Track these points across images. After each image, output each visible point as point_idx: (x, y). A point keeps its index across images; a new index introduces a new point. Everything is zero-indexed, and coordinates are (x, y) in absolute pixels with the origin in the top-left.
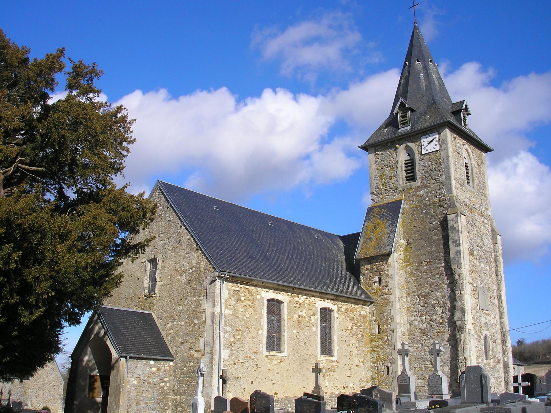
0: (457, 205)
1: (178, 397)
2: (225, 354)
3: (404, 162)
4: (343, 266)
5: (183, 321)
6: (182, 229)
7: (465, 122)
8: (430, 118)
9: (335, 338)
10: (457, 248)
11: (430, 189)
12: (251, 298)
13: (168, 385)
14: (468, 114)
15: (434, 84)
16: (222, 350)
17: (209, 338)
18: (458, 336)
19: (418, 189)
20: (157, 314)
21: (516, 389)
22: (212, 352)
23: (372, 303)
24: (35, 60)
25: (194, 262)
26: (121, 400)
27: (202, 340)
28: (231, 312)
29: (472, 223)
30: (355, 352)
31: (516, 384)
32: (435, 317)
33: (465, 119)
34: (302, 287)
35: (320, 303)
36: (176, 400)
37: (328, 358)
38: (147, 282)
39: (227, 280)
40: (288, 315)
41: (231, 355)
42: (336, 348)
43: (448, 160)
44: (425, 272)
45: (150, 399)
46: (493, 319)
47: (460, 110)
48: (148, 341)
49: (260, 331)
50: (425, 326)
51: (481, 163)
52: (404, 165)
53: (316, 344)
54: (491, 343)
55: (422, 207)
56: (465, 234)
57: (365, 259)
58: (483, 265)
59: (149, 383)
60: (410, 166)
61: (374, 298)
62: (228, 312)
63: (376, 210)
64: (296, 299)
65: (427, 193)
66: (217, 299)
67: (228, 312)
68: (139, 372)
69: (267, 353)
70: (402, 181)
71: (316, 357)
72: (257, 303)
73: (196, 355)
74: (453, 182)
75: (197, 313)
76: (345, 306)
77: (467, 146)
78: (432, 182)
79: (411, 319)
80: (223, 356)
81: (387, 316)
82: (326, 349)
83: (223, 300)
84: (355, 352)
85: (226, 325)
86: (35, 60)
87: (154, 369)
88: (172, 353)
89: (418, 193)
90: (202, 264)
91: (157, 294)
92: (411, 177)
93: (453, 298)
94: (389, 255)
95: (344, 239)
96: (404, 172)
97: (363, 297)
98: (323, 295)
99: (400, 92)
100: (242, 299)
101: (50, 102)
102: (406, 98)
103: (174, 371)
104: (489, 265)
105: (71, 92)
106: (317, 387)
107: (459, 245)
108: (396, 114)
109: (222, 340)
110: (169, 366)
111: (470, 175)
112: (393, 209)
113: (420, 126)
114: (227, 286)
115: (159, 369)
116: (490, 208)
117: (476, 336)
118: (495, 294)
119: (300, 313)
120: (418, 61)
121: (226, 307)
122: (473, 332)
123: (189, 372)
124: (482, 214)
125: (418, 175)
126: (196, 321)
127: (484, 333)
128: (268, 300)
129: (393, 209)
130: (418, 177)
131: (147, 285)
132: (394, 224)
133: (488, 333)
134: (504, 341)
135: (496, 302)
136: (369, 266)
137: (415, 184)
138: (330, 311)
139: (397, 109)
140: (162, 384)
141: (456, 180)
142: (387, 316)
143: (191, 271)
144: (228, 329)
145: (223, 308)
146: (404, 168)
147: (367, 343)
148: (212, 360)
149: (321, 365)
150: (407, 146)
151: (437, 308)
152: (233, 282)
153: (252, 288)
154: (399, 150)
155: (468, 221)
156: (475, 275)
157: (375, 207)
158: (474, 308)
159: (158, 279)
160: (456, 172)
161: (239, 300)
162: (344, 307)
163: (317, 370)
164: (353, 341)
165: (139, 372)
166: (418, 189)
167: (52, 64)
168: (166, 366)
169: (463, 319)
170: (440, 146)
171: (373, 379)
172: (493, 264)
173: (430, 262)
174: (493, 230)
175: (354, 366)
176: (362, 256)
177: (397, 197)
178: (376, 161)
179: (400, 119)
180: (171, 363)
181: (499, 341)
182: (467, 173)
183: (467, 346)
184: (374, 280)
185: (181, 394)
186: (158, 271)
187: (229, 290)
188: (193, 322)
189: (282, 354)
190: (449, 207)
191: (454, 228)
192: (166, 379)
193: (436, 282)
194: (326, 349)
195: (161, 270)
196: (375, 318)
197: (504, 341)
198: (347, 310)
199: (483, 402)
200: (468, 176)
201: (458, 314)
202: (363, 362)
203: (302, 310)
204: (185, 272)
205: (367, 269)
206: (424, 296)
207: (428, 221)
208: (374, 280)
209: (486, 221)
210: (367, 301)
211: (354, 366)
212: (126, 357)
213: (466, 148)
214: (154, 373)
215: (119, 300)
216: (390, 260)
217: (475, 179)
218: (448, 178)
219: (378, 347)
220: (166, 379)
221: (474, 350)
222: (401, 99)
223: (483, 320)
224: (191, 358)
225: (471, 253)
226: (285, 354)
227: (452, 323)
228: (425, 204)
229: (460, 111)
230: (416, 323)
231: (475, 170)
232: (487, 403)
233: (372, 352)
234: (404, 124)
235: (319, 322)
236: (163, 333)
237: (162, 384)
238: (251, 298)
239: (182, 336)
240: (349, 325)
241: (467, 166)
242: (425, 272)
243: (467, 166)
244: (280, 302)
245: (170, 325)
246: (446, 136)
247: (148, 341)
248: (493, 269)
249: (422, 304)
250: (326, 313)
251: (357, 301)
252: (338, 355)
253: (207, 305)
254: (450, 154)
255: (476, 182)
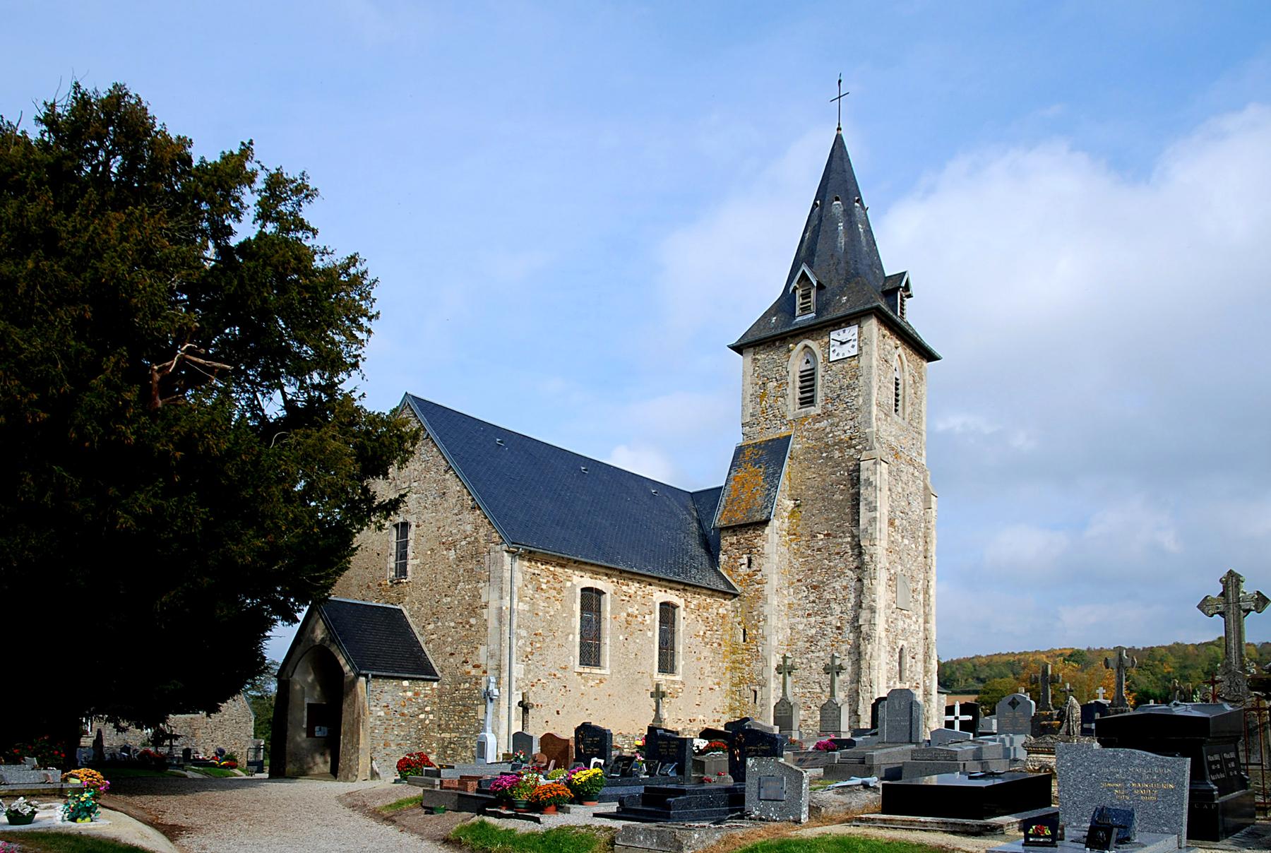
0: (877, 445)
1: (447, 735)
2: (518, 670)
3: (798, 374)
4: (685, 538)
5: (452, 620)
6: (447, 476)
7: (902, 309)
8: (848, 300)
9: (680, 648)
10: (873, 514)
11: (836, 420)
12: (558, 586)
13: (431, 716)
14: (909, 296)
15: (860, 242)
16: (514, 665)
17: (494, 647)
18: (862, 648)
19: (818, 418)
20: (410, 610)
21: (950, 725)
22: (499, 668)
23: (735, 596)
24: (203, 160)
25: (469, 528)
26: (361, 741)
27: (482, 649)
28: (526, 607)
29: (896, 475)
30: (708, 668)
31: (951, 718)
32: (830, 618)
33: (902, 305)
34: (635, 570)
35: (660, 595)
36: (443, 739)
37: (670, 677)
38: (393, 559)
39: (522, 557)
40: (612, 613)
41: (527, 671)
42: (680, 663)
43: (869, 373)
44: (819, 550)
45: (405, 738)
46: (915, 624)
47: (896, 289)
48: (397, 651)
49: (571, 637)
50: (813, 631)
51: (918, 379)
52: (798, 379)
53: (653, 657)
54: (908, 658)
55: (823, 449)
56: (886, 492)
57: (727, 528)
58: (906, 542)
59: (403, 714)
60: (808, 380)
61: (739, 589)
62: (522, 606)
63: (748, 452)
64: (625, 588)
65: (832, 425)
66: (507, 587)
67: (522, 606)
68: (387, 698)
69: (581, 670)
70: (791, 406)
71: (652, 676)
72: (565, 593)
73: (473, 672)
74: (874, 409)
75: (474, 608)
76: (696, 600)
77: (900, 350)
78: (841, 407)
79: (793, 620)
80: (514, 674)
81: (758, 615)
82: (667, 665)
83: (515, 589)
84: (708, 668)
85: (519, 626)
86: (203, 160)
87: (409, 694)
88: (436, 669)
89: (817, 425)
90: (482, 532)
91: (409, 579)
92: (807, 401)
93: (860, 593)
94: (766, 522)
95: (696, 496)
96: (798, 390)
97: (722, 587)
98: (668, 583)
99: (803, 254)
100: (544, 586)
101: (234, 242)
102: (810, 266)
103: (440, 697)
104: (916, 543)
105: (263, 226)
106: (658, 717)
107: (875, 509)
108: (794, 291)
109: (514, 649)
110: (432, 689)
111: (900, 398)
112: (775, 451)
113: (826, 317)
114: (522, 566)
115: (416, 694)
116: (924, 453)
117: (888, 648)
118: (920, 587)
119: (630, 610)
120: (837, 199)
121: (520, 600)
122: (884, 642)
123: (462, 698)
124: (911, 462)
125: (820, 395)
126: (473, 621)
127: (901, 643)
128: (583, 590)
129: (775, 451)
130: (819, 400)
131: (393, 565)
132: (776, 475)
133: (905, 643)
134: (927, 657)
135: (921, 597)
136: (734, 540)
137: (815, 410)
138: (675, 607)
139: (794, 284)
140: (422, 716)
141: (879, 405)
142: (758, 615)
143: (464, 543)
144: (523, 633)
145: (515, 601)
146: (798, 384)
147: (725, 656)
148: (499, 678)
149: (663, 688)
150: (806, 346)
151: (833, 605)
152: (529, 560)
153: (559, 570)
154: (793, 354)
155: (890, 473)
156: (894, 557)
157: (749, 446)
158: (889, 607)
159: (410, 554)
160: (880, 393)
161: (539, 589)
162: (695, 602)
163: (658, 695)
164: (706, 652)
165: (387, 698)
166: (818, 418)
167: (232, 172)
168: (428, 689)
169: (872, 624)
170: (860, 348)
171: (732, 709)
172: (921, 541)
173: (828, 535)
174: (926, 488)
175: (706, 691)
176: (723, 523)
177: (784, 431)
178: (755, 371)
179: (799, 301)
180: (435, 685)
181: (920, 657)
182: (897, 395)
183: (875, 663)
184: (741, 561)
185: (452, 731)
186: (411, 543)
187: (524, 573)
188: (468, 622)
189: (603, 672)
190: (865, 449)
191: (869, 483)
192: (428, 709)
193: (835, 567)
194: (667, 665)
195: (415, 541)
196: (739, 619)
197: (927, 657)
198: (699, 607)
199: (911, 742)
200: (897, 400)
201: (865, 615)
202: (718, 684)
203: (632, 605)
204: (454, 544)
205: (731, 544)
206: (815, 587)
207: (829, 470)
208: (741, 561)
209: (917, 474)
210: (729, 593)
211: (706, 691)
212: (366, 676)
213: (899, 352)
214: (410, 699)
215: (352, 587)
216: (767, 530)
217: (907, 404)
218: (867, 402)
219: (743, 662)
220: (428, 709)
221: (884, 667)
222: (804, 268)
223: (900, 623)
224: (466, 677)
225: (891, 523)
226: (606, 671)
227: (857, 629)
228: (827, 444)
229: (896, 290)
230: (801, 627)
231: (910, 391)
232: (917, 743)
233: (733, 669)
234: (805, 310)
235: (657, 624)
236: (420, 639)
237: (422, 716)
238: (558, 586)
239: (452, 643)
240: (701, 628)
241: (897, 384)
242: (819, 550)
243: (897, 384)
244: (600, 593)
245: (431, 626)
246: (871, 330)
247: (397, 651)
248: (921, 548)
249: (812, 599)
250: (668, 611)
251: (714, 592)
252: (684, 673)
253: (488, 594)
254: (875, 363)
255: (909, 410)
